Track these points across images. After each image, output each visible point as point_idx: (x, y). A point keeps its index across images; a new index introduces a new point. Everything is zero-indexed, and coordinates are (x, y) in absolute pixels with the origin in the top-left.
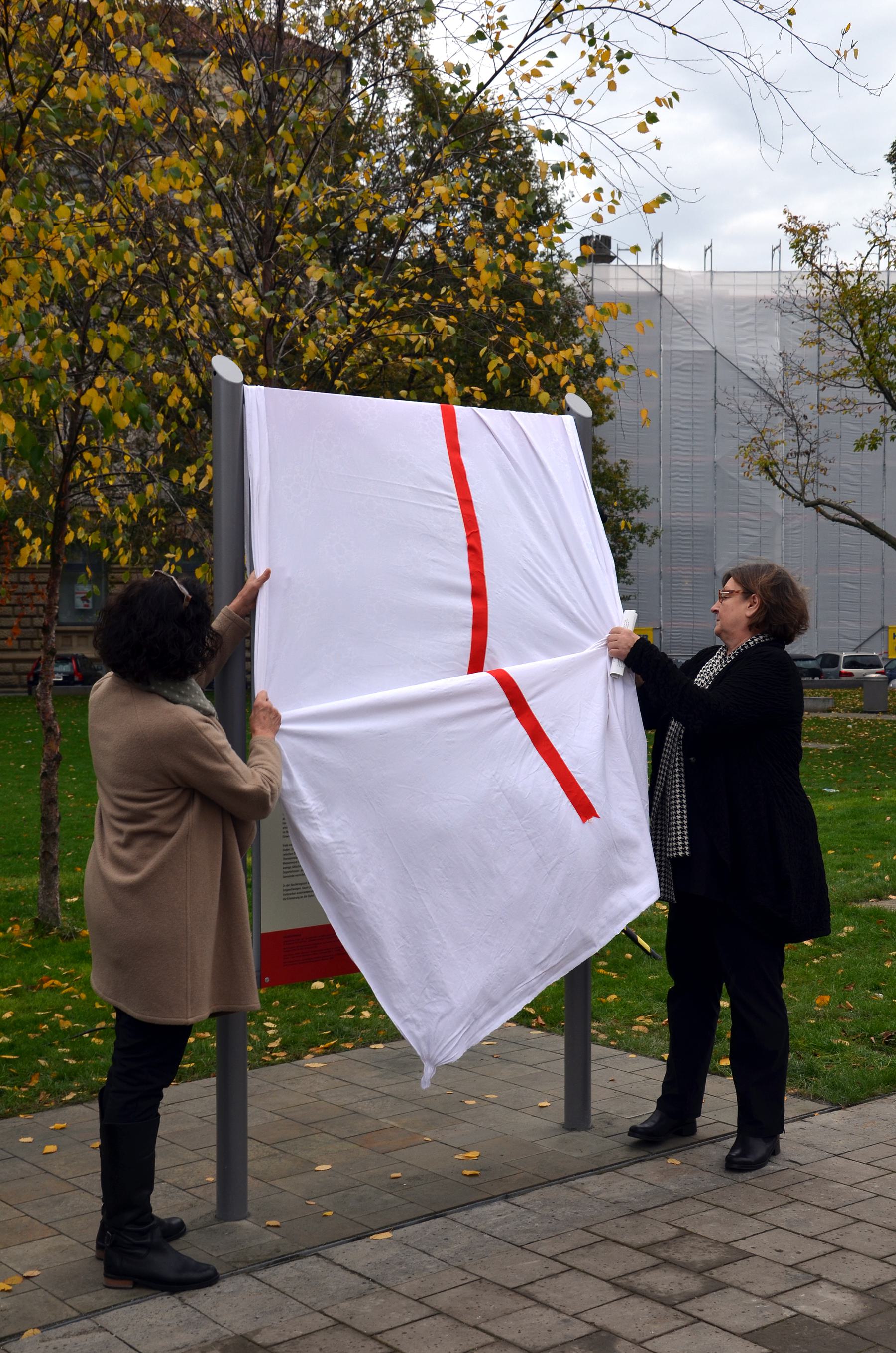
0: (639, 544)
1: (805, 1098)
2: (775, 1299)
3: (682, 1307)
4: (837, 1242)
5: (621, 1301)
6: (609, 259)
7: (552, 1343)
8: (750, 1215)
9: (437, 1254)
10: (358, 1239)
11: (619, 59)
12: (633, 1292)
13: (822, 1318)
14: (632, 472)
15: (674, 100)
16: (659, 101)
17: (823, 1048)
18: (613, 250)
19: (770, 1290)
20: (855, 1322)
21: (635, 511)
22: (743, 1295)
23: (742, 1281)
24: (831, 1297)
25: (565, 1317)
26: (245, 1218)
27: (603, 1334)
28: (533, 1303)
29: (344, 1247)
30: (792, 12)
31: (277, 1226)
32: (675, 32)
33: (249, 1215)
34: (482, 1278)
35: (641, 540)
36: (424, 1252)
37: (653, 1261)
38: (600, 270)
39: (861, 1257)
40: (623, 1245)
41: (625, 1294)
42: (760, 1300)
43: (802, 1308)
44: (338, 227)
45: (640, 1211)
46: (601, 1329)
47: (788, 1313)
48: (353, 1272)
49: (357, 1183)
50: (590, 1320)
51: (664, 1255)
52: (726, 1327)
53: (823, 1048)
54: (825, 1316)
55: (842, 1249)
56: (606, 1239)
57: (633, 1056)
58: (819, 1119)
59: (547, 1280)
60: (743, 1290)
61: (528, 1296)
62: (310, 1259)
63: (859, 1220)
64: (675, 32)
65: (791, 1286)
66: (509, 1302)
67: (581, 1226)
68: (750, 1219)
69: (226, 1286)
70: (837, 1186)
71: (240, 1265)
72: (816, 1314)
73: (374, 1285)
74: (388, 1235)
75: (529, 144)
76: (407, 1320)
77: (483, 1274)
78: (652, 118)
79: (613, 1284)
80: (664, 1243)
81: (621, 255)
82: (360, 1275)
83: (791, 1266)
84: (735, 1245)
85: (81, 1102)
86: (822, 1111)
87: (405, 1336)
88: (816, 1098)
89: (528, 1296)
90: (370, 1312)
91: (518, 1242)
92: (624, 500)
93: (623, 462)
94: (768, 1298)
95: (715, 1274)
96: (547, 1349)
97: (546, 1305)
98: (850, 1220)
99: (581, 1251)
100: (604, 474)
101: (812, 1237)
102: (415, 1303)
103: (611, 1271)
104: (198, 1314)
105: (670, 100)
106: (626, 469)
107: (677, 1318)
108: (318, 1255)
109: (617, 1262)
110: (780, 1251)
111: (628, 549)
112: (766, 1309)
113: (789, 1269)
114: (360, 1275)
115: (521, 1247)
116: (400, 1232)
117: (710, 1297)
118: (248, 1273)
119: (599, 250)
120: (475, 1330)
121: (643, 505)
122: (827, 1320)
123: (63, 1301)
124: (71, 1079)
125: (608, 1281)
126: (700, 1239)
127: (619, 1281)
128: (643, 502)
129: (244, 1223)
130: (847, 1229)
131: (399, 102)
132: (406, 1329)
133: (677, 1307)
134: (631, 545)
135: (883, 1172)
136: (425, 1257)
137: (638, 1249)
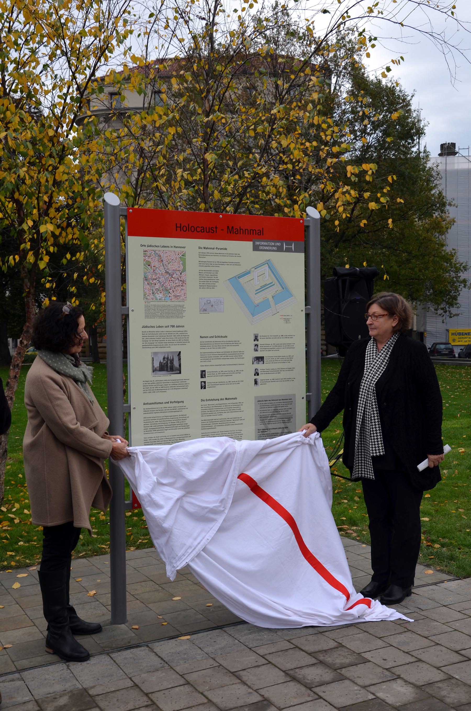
0: (463, 289)
1: (443, 573)
2: (368, 688)
3: (315, 690)
4: (419, 657)
5: (285, 684)
6: (454, 153)
7: (236, 706)
8: (380, 638)
9: (206, 650)
10: (173, 638)
11: (370, 41)
12: (294, 679)
13: (387, 701)
14: (458, 254)
15: (401, 60)
16: (393, 61)
17: (465, 545)
18: (457, 149)
19: (367, 682)
20: (405, 705)
21: (461, 273)
22: (352, 684)
23: (356, 676)
24: (399, 689)
25: (251, 691)
26: (124, 623)
27: (265, 703)
28: (240, 681)
29: (162, 642)
30: (454, 7)
31: (137, 629)
32: (402, 25)
33: (127, 621)
34: (221, 665)
35: (465, 287)
36: (200, 648)
37: (314, 661)
38: (450, 158)
39: (428, 666)
40: (303, 651)
41: (290, 680)
42: (359, 688)
43: (381, 695)
44: (325, 147)
45: (323, 632)
46: (265, 699)
47: (371, 697)
48: (159, 657)
49: (189, 608)
50: (262, 694)
51: (321, 658)
52: (333, 703)
53: (465, 545)
54: (391, 700)
55: (420, 660)
56: (297, 647)
57: (364, 546)
58: (446, 584)
59: (253, 669)
60: (353, 682)
61: (238, 678)
62: (142, 648)
63: (438, 644)
64: (402, 25)
65: (381, 681)
66: (228, 679)
67: (288, 638)
68: (378, 640)
69: (93, 661)
70: (436, 623)
71: (107, 649)
72: (387, 699)
73: (166, 665)
74: (188, 637)
75: (409, 101)
76: (170, 686)
77: (222, 662)
78: (388, 69)
79: (286, 673)
80: (326, 651)
81: (461, 151)
82: (162, 659)
83: (387, 669)
84: (363, 655)
85: (85, 557)
86: (450, 580)
87: (163, 696)
88: (449, 573)
89: (238, 678)
90: (153, 682)
91: (250, 646)
92: (456, 268)
93: (454, 250)
94: (364, 687)
95: (344, 671)
96: (231, 709)
97: (244, 683)
98: (433, 644)
99: (280, 653)
100: (444, 256)
101: (407, 653)
102: (179, 677)
103: (288, 666)
104: (71, 675)
105: (399, 61)
106: (455, 252)
107: (309, 696)
108: (147, 646)
109: (291, 661)
110: (385, 660)
111: (458, 291)
112: (359, 694)
113: (385, 671)
114: (162, 659)
115: (250, 649)
116: (195, 636)
117: (333, 685)
118: (108, 654)
119: (448, 150)
120: (200, 695)
121: (465, 270)
122: (390, 703)
123: (13, 662)
124: (88, 545)
125: (284, 671)
126: (346, 650)
127: (290, 672)
128: (465, 268)
129: (123, 626)
130: (428, 649)
131: (347, 85)
132: (166, 692)
133: (313, 689)
134: (460, 289)
135: (466, 616)
136: (199, 651)
137: (310, 654)
